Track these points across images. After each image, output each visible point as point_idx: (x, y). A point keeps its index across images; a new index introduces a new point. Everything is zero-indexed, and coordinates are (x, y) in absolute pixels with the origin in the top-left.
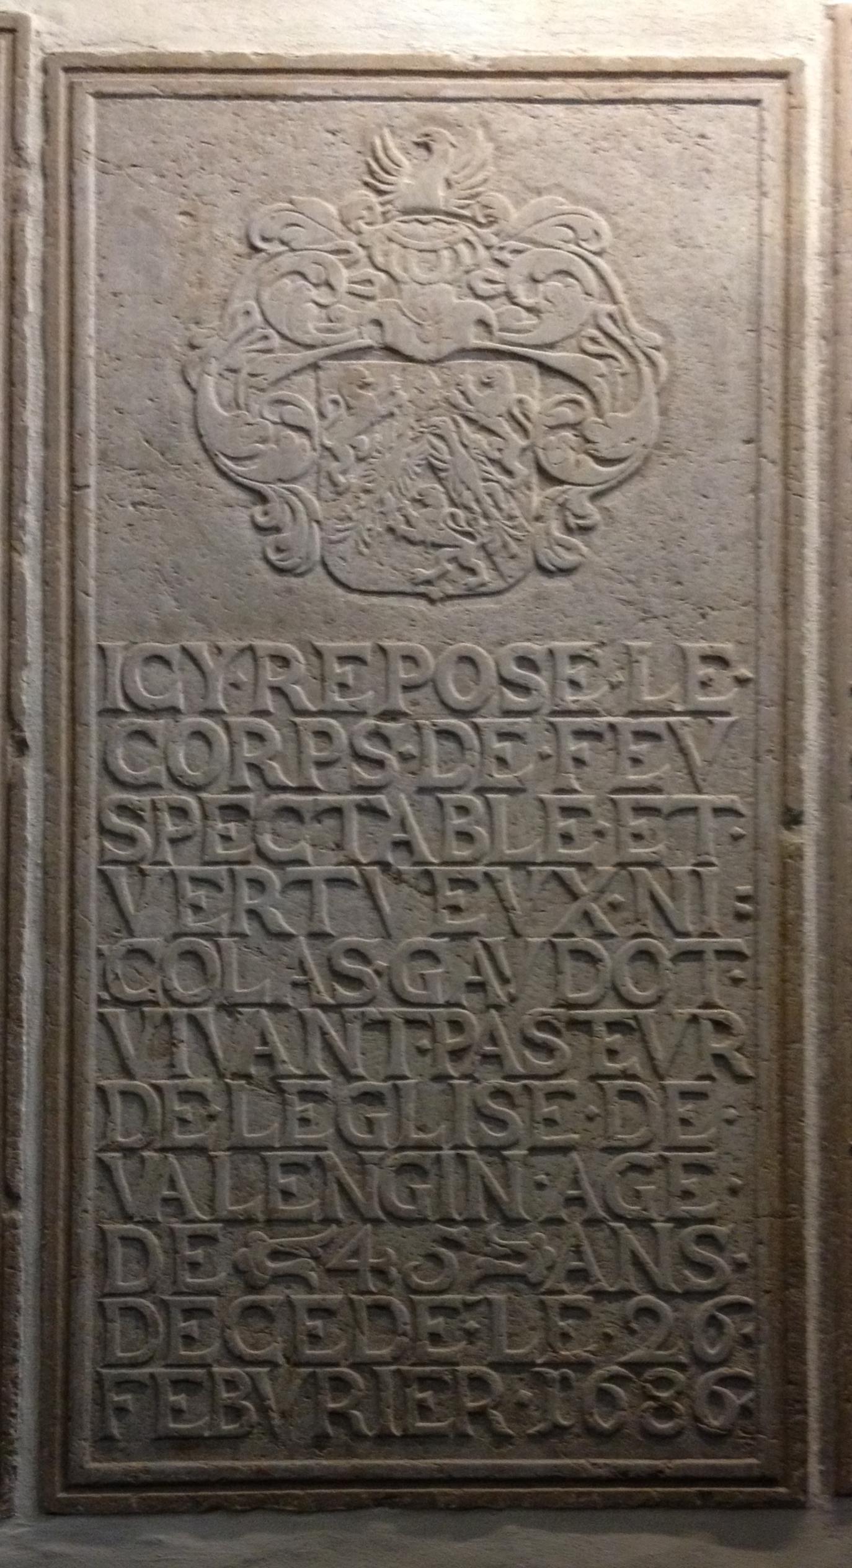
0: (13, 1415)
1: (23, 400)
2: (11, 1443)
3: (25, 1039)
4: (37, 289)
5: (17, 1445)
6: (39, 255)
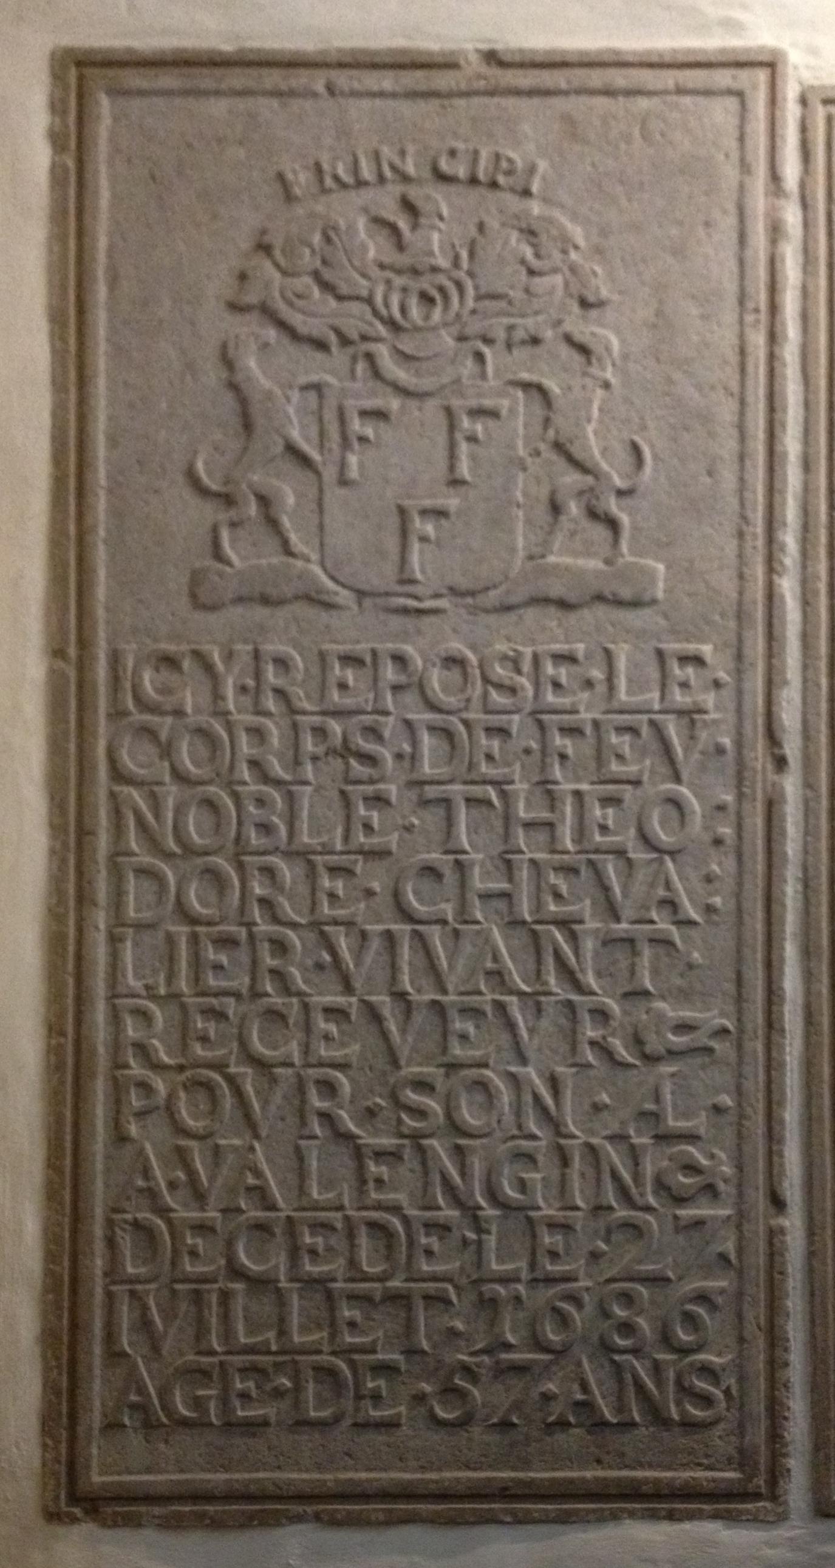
0: (786, 1418)
1: (784, 426)
2: (786, 1445)
3: (788, 1049)
4: (798, 319)
5: (790, 1448)
6: (799, 284)
